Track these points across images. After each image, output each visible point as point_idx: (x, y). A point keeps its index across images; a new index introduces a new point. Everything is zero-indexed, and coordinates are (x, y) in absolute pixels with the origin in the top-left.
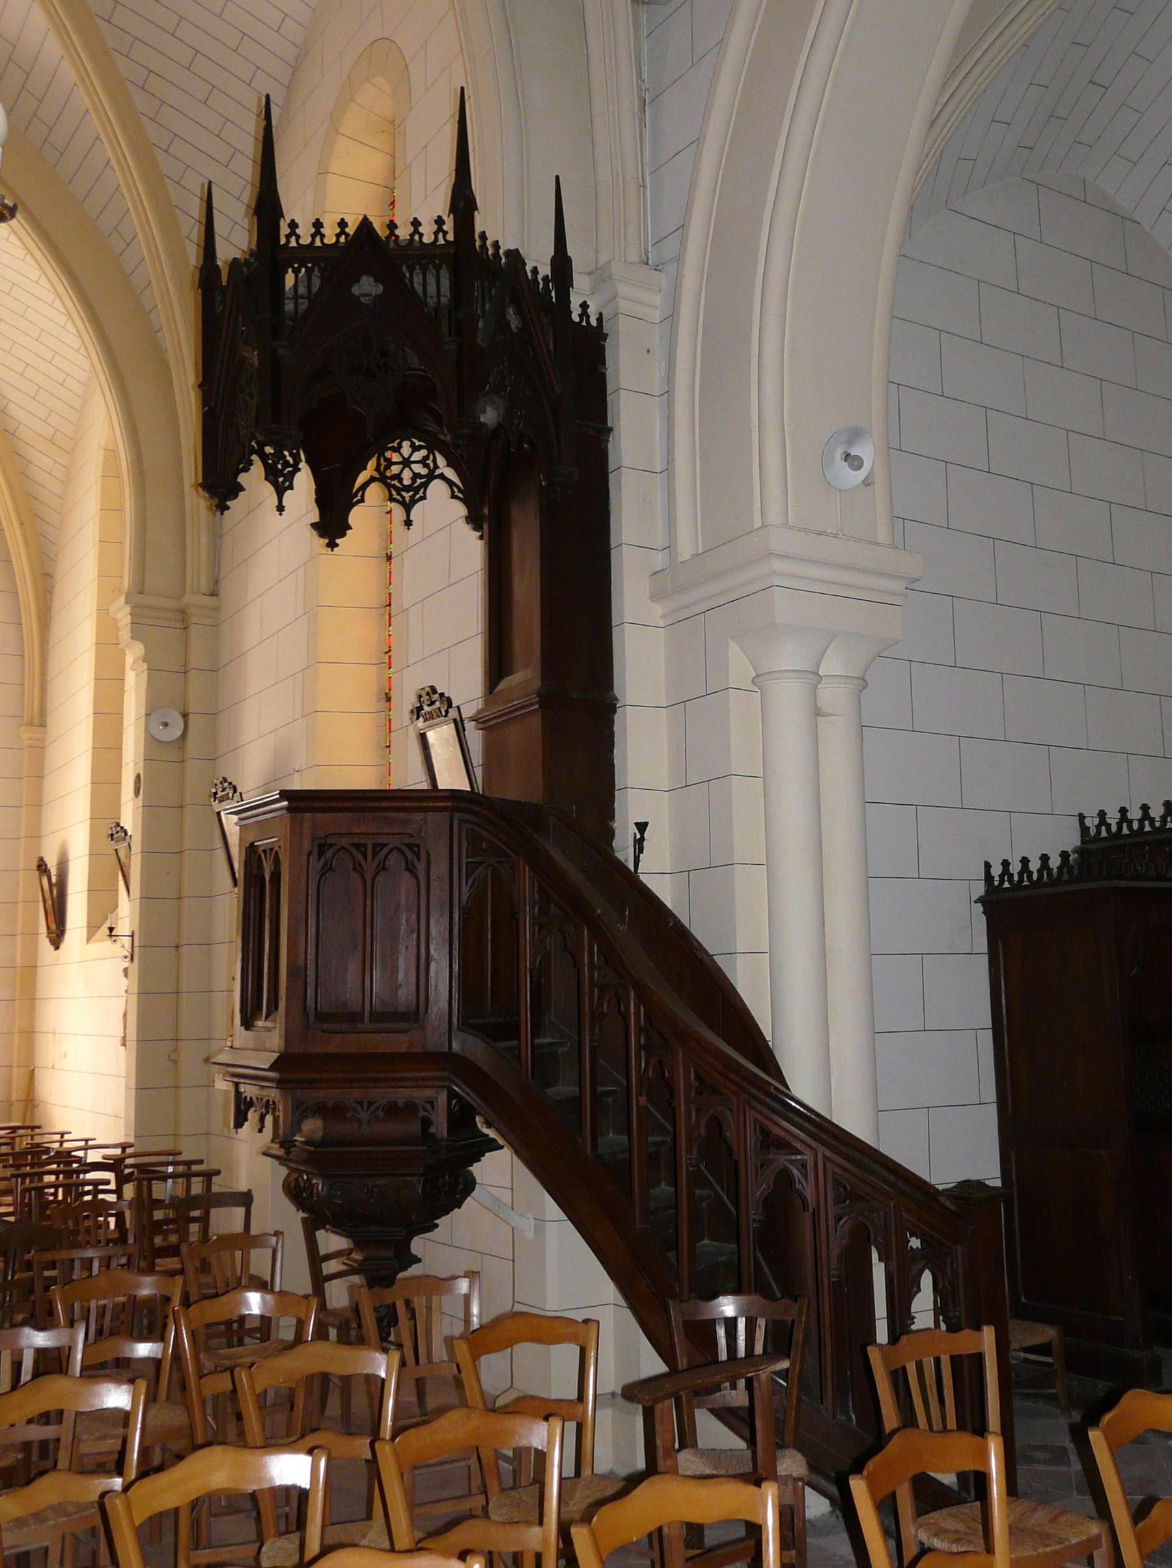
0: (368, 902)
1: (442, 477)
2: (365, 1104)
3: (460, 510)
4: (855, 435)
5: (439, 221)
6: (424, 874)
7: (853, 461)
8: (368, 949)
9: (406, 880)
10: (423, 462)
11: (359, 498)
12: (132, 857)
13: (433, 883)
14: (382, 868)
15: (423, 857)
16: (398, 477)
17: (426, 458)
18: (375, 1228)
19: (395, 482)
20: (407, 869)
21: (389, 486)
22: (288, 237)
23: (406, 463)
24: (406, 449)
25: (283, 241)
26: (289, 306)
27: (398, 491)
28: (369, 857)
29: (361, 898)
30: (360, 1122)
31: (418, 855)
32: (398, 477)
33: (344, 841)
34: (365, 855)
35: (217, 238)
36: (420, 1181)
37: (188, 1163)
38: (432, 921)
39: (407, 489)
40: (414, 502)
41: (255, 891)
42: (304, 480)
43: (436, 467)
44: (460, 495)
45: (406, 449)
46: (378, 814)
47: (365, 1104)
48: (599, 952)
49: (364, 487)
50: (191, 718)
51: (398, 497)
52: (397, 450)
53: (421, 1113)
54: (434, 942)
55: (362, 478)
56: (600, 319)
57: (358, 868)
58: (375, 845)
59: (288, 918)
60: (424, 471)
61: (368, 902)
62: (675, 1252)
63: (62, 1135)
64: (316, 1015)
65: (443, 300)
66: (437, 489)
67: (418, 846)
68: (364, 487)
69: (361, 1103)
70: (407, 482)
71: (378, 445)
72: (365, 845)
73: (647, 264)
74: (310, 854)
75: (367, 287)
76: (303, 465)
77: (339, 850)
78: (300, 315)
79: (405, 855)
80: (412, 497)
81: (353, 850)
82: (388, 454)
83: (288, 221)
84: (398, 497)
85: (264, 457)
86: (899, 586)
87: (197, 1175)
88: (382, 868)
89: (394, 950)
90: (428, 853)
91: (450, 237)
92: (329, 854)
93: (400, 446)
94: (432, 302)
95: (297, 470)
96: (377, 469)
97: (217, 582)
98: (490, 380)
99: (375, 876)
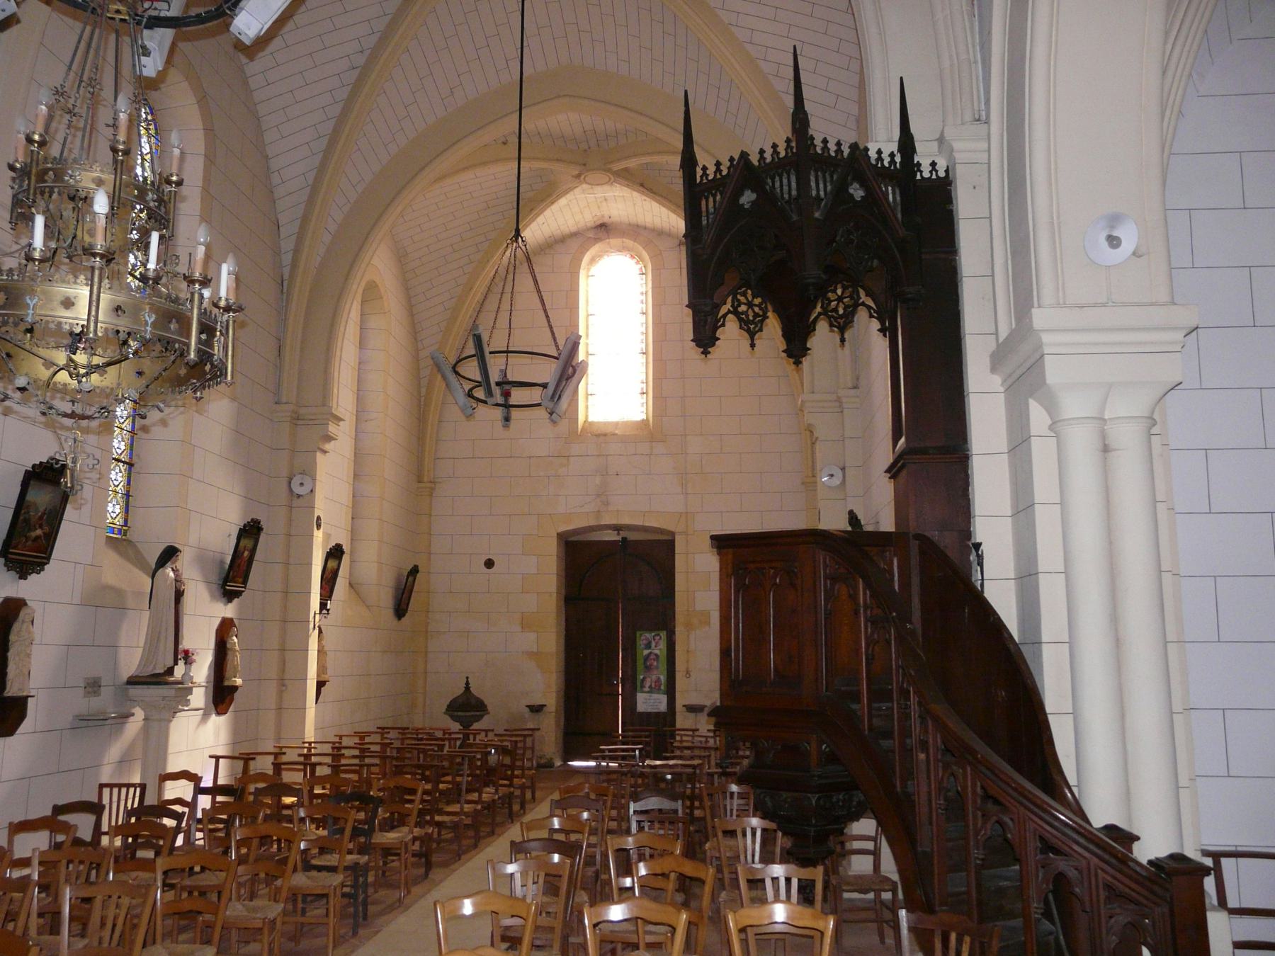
1: (863, 304)
4: (1115, 220)
5: (892, 155)
7: (1114, 241)
21: (829, 317)
22: (701, 177)
25: (698, 181)
27: (836, 319)
48: (871, 596)
49: (725, 316)
55: (724, 310)
56: (947, 171)
59: (659, 540)
68: (725, 316)
70: (841, 311)
71: (822, 290)
73: (979, 120)
75: (747, 198)
76: (770, 314)
83: (701, 167)
84: (835, 323)
86: (1179, 336)
95: (765, 317)
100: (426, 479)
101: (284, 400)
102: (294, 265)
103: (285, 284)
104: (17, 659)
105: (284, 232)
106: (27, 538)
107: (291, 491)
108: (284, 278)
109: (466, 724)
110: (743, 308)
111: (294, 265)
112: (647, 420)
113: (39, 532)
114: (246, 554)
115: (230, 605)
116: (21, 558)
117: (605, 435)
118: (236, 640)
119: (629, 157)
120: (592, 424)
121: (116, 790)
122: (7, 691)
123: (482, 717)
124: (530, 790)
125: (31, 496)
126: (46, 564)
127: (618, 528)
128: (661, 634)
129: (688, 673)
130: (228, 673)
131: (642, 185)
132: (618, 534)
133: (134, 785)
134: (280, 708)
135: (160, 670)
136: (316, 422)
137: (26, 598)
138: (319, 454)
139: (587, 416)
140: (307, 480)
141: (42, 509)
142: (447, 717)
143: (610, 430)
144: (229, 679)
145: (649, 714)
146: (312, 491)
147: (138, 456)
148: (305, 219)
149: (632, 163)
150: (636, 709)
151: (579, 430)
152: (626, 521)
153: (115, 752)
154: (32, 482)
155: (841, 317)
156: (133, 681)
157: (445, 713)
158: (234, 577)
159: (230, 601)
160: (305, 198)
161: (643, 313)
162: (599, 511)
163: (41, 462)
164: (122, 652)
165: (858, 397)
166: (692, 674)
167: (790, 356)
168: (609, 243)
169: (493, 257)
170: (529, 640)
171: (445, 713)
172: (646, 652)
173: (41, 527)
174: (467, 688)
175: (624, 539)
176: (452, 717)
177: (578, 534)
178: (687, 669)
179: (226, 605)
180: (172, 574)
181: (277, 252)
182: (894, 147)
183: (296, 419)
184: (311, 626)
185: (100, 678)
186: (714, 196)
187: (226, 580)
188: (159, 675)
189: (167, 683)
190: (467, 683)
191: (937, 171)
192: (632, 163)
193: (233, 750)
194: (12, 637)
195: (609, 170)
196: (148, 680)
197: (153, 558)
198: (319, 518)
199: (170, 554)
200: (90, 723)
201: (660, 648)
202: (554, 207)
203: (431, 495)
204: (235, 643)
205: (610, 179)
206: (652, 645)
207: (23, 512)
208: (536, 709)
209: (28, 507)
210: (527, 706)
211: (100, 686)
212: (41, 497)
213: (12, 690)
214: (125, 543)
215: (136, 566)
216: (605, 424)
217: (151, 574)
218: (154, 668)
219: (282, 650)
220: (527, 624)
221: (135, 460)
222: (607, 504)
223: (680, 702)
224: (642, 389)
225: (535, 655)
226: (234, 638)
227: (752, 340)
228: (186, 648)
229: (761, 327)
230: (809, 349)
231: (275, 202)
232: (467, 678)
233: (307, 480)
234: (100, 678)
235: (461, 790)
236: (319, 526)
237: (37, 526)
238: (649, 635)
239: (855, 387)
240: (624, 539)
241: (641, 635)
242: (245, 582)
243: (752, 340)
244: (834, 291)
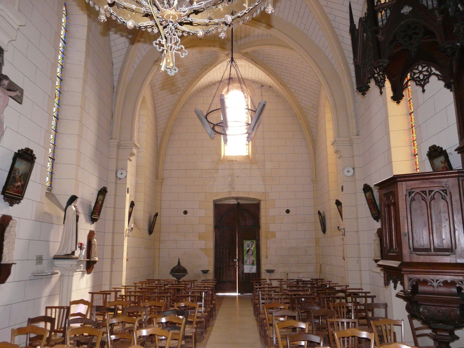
0: (429, 210)
1: (434, 74)
2: (435, 281)
3: (442, 83)
6: (449, 199)
8: (430, 227)
9: (443, 203)
10: (427, 71)
11: (406, 86)
12: (342, 208)
13: (454, 203)
14: (433, 198)
15: (448, 193)
16: (419, 77)
17: (428, 69)
18: (441, 324)
19: (418, 79)
20: (442, 198)
23: (421, 72)
24: (420, 68)
25: (376, 4)
26: (380, 24)
27: (419, 81)
28: (428, 195)
29: (426, 209)
30: (434, 287)
31: (446, 193)
32: (419, 77)
33: (418, 190)
34: (426, 194)
35: (354, 16)
36: (458, 310)
37: (366, 293)
38: (455, 216)
39: (422, 80)
40: (425, 84)
41: (387, 209)
42: (388, 84)
43: (431, 71)
44: (441, 78)
45: (420, 68)
46: (430, 180)
47: (435, 281)
49: (407, 82)
50: (355, 169)
51: (419, 83)
52: (417, 69)
53: (458, 285)
54: (456, 224)
57: (423, 199)
58: (429, 191)
59: (253, 204)
61: (429, 210)
63: (329, 282)
64: (413, 248)
65: (435, 5)
66: (433, 79)
67: (446, 190)
68: (407, 82)
69: (433, 280)
72: (426, 191)
74: (406, 195)
76: (386, 79)
77: (416, 194)
78: (384, 24)
79: (441, 194)
80: (424, 82)
81: (422, 193)
82: (414, 71)
84: (419, 83)
85: (375, 78)
87: (369, 297)
88: (433, 198)
89: (440, 226)
90: (450, 192)
92: (413, 195)
93: (418, 67)
94: (430, 7)
96: (411, 76)
97: (358, 132)
98: (455, 28)
99: (431, 201)
100: (159, 178)
101: (114, 138)
102: (119, 82)
103: (115, 88)
104: (8, 245)
105: (115, 67)
106: (14, 186)
107: (117, 176)
108: (115, 86)
109: (179, 278)
110: (376, 75)
111: (119, 82)
112: (249, 155)
113: (19, 184)
114: (100, 202)
115: (93, 225)
116: (11, 195)
117: (232, 161)
118: (96, 240)
119: (248, 47)
120: (227, 156)
121: (62, 310)
122: (2, 261)
123: (185, 275)
124: (371, 312)
125: (17, 165)
126: (22, 199)
127: (237, 198)
128: (254, 241)
129: (267, 257)
130: (93, 255)
131: (252, 60)
132: (237, 201)
133: (56, 308)
134: (111, 271)
135: (70, 253)
136: (128, 147)
137: (12, 216)
138: (128, 161)
139: (224, 154)
140: (124, 172)
141: (21, 172)
142: (170, 275)
143: (234, 159)
144: (93, 258)
145: (249, 274)
146: (126, 177)
147: (57, 156)
148: (124, 62)
149: (249, 50)
151: (222, 159)
152: (241, 195)
153: (47, 291)
154: (18, 159)
156: (56, 258)
157: (170, 274)
158: (95, 212)
159: (93, 223)
160: (125, 52)
161: (247, 113)
162: (230, 191)
163: (22, 149)
164: (51, 244)
165: (359, 139)
166: (268, 257)
168: (233, 86)
169: (189, 88)
170: (202, 244)
171: (170, 274)
172: (248, 249)
173: (20, 181)
174: (179, 263)
175: (238, 203)
176: (174, 276)
177: (220, 201)
178: (267, 255)
179: (91, 224)
180: (74, 208)
181: (112, 74)
183: (119, 146)
184: (125, 235)
185: (42, 256)
186: (381, 12)
187: (93, 213)
188: (68, 255)
189: (72, 259)
190: (179, 261)
192: (249, 50)
193: (93, 290)
194: (6, 234)
195: (240, 53)
196: (62, 257)
197: (64, 201)
198: (128, 189)
199: (73, 199)
200: (38, 277)
201: (253, 248)
202: (214, 69)
203: (161, 185)
204: (95, 241)
205: (240, 56)
206: (249, 245)
207: (13, 173)
208: (205, 272)
209: (16, 170)
210: (202, 271)
211: (42, 260)
212: (21, 166)
213: (5, 260)
214: (51, 194)
215: (56, 205)
216: (232, 156)
217: (64, 210)
218: (67, 251)
219: (113, 245)
220: (201, 237)
221: (55, 158)
222: (233, 188)
223: (264, 268)
224: (247, 143)
225: (205, 250)
226: (95, 239)
227: (381, 90)
228: (81, 242)
231: (112, 54)
232: (179, 259)
233: (124, 172)
234: (42, 256)
235: (204, 306)
236: (128, 192)
237: (19, 181)
238: (249, 242)
239: (358, 135)
240: (238, 203)
241: (245, 242)
242: (99, 215)
243: (381, 90)
244: (423, 67)
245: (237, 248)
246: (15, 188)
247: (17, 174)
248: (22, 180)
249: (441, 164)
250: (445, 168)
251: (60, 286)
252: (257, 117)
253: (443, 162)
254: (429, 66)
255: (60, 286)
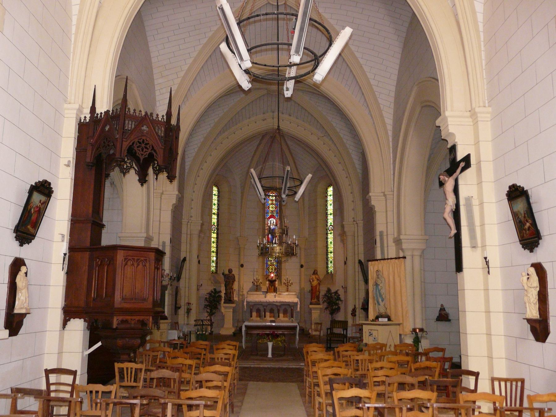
1: (134, 168)
5: (163, 116)
43: (133, 165)
58: (137, 259)
60: (129, 165)
62: (67, 408)
66: (132, 172)
91: (165, 120)
106: (525, 230)
113: (528, 224)
141: (522, 212)
150: (114, 306)
155: (157, 170)
167: (139, 182)
173: (527, 222)
182: (164, 113)
191: (158, 118)
229: (129, 171)
230: (147, 181)
245: (456, 380)
246: (527, 231)
247: (520, 217)
248: (528, 219)
249: (39, 200)
250: (38, 209)
251: (154, 283)
252: (224, 54)
253: (42, 203)
254: (132, 161)
255: (154, 283)
